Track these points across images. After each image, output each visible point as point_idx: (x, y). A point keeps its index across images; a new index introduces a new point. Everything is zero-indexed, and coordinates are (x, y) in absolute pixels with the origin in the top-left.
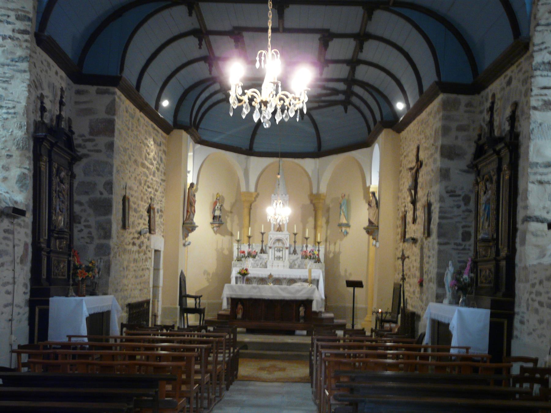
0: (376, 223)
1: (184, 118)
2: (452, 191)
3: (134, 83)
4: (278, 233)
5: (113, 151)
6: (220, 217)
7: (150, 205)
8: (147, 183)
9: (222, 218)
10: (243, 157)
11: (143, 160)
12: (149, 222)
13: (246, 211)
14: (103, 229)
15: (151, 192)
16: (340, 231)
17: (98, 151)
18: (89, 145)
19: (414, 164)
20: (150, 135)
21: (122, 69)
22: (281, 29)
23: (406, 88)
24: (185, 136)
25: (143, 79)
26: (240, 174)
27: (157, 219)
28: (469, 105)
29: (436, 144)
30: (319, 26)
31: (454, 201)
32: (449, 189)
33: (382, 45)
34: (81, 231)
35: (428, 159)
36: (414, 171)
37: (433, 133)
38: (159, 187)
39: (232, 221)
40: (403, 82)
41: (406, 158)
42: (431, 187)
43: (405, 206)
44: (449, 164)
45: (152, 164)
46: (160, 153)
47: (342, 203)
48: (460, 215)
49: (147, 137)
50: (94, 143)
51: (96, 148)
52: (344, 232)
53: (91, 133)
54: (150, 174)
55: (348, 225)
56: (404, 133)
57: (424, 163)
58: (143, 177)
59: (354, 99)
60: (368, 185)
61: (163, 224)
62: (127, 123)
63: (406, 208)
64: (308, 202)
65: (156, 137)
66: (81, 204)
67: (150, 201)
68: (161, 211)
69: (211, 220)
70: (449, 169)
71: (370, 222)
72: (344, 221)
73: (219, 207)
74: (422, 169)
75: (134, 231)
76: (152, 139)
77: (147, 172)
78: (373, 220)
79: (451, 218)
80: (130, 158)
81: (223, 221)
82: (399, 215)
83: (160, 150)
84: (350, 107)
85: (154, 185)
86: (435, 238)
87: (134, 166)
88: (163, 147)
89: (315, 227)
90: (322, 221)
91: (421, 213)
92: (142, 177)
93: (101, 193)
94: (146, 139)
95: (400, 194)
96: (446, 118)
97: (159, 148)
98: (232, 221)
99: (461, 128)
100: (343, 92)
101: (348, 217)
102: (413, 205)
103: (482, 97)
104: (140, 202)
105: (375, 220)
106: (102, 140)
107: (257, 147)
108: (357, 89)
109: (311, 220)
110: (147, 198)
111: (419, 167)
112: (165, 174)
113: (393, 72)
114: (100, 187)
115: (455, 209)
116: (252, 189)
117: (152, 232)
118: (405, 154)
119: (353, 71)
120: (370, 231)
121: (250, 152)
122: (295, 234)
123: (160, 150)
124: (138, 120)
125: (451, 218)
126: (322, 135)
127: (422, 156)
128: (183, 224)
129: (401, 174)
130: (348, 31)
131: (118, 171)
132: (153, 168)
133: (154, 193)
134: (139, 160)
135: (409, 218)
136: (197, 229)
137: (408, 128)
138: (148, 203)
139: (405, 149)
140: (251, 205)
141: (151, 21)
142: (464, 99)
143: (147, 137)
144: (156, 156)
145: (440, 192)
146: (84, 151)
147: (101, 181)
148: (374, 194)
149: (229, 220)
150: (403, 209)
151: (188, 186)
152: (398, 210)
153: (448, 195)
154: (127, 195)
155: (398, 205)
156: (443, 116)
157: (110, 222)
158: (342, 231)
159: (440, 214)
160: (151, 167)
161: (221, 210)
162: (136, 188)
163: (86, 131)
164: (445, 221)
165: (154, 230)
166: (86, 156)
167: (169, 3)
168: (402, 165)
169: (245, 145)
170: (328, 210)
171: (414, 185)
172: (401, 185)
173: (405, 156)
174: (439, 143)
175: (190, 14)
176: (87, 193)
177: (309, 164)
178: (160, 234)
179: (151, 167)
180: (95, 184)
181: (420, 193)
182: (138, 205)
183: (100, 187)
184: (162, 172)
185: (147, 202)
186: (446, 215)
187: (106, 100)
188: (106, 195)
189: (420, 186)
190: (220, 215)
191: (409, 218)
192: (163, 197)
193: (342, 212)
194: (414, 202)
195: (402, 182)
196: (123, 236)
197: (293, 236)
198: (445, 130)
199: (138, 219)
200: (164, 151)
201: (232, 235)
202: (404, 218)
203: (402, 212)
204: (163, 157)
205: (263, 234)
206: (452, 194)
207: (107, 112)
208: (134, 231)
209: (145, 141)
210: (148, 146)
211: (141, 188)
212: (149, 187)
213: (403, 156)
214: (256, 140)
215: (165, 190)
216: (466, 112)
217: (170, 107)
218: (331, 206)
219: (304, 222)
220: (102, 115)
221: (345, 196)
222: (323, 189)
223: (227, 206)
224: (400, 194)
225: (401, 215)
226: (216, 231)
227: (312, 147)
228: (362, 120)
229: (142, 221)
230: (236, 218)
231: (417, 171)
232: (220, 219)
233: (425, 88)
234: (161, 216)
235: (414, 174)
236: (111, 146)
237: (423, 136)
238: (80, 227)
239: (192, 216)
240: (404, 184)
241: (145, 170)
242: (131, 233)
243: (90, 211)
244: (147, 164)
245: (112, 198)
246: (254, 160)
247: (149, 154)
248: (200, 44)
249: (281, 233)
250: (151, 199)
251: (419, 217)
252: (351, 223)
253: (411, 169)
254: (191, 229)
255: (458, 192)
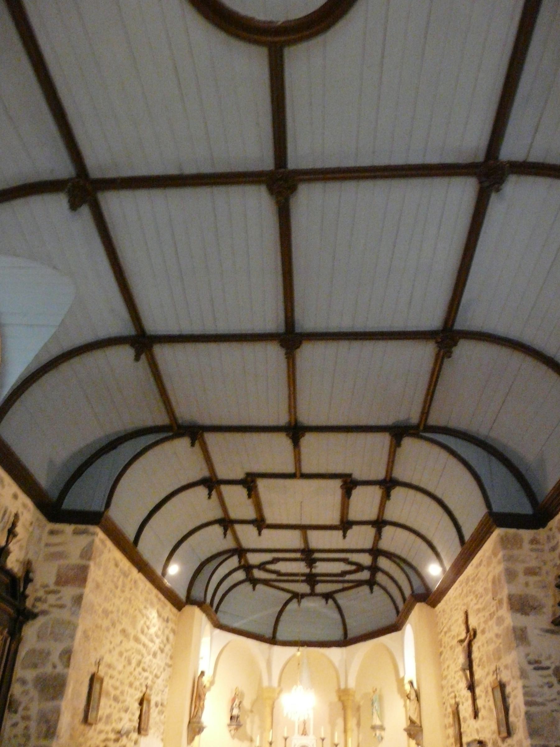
0: (418, 721)
1: (198, 593)
2: (536, 662)
3: (131, 537)
4: (303, 737)
5: (80, 607)
6: (238, 717)
7: (144, 695)
8: (142, 665)
9: (240, 719)
10: (265, 646)
11: (137, 632)
12: (140, 717)
13: (268, 710)
14: (47, 721)
15: (146, 678)
16: (374, 735)
17: (62, 607)
18: (52, 599)
19: (463, 635)
20: (152, 604)
21: (108, 505)
22: (298, 475)
23: (439, 549)
24: (197, 611)
25: (144, 531)
26: (263, 665)
27: (154, 714)
28: (534, 541)
29: (499, 597)
30: (340, 469)
31: (541, 676)
32: (532, 657)
33: (412, 492)
34: (15, 725)
35: (486, 622)
36: (466, 643)
37: (490, 585)
38: (161, 673)
39: (252, 722)
40: (435, 543)
41: (448, 635)
42: (499, 659)
43: (455, 697)
44: (523, 620)
45: (152, 641)
46: (167, 632)
47: (374, 699)
48: (555, 699)
49: (148, 606)
50: (58, 596)
51: (59, 602)
52: (378, 737)
53: (57, 583)
54: (149, 654)
55: (382, 728)
56: (440, 606)
57: (478, 632)
58: (134, 654)
59: (380, 577)
60: (401, 675)
61: (164, 723)
62: (115, 579)
63: (457, 700)
64: (335, 698)
65: (161, 610)
66: (24, 682)
67: (144, 689)
68: (162, 705)
69: (228, 720)
70: (526, 628)
71: (412, 722)
72: (377, 722)
73: (238, 704)
74: (476, 640)
75: (109, 728)
76: (156, 611)
77: (144, 651)
78: (415, 718)
79: (543, 704)
80: (113, 624)
81: (242, 722)
82: (446, 710)
83: (167, 627)
84: (376, 588)
85: (153, 668)
86: (523, 737)
87: (120, 638)
88: (171, 625)
89: (345, 731)
90: (352, 723)
91: (485, 702)
92: (133, 653)
93: (54, 667)
94: (145, 607)
95: (444, 682)
96: (509, 559)
97: (165, 624)
98: (252, 722)
99: (530, 572)
100: (369, 568)
101: (381, 717)
102: (471, 692)
103: (551, 529)
104: (126, 688)
105: (417, 718)
106: (68, 592)
107: (280, 636)
108: (383, 562)
109: (340, 722)
110: (141, 684)
111: (472, 637)
112: (171, 658)
113: (423, 531)
114: (55, 657)
115: (546, 689)
116: (275, 683)
117: (142, 732)
118: (445, 629)
119: (378, 535)
120: (412, 733)
121: (273, 640)
122: (323, 740)
123: (167, 627)
124: (135, 582)
125: (543, 704)
126: (347, 621)
127: (473, 623)
128: (189, 722)
129: (442, 656)
130: (373, 477)
131: (86, 636)
132: (154, 647)
133: (153, 679)
134: (131, 632)
135: (466, 710)
136: (205, 730)
137: (446, 598)
138: (141, 692)
139: (444, 625)
140: (273, 704)
141: (150, 454)
142: (526, 534)
143: (148, 606)
144: (160, 633)
145: (519, 663)
146: (44, 607)
147: (56, 649)
148: (411, 683)
149: (248, 721)
150: (453, 702)
151: (199, 673)
152: (444, 703)
153: (532, 667)
154: (99, 672)
155: (443, 697)
156: (504, 556)
157: (57, 712)
158: (375, 735)
159: (527, 698)
160: (151, 645)
161: (239, 708)
162: (120, 667)
163: (51, 580)
164: (533, 709)
165: (146, 730)
166: (44, 613)
167: (171, 434)
168: (443, 645)
169: (268, 633)
170: (358, 709)
171: (467, 663)
172: (444, 670)
173: (446, 633)
174: (504, 594)
175: (193, 445)
176: (35, 666)
177: (335, 653)
178: (158, 737)
179: (151, 645)
180: (48, 654)
181: (478, 673)
182: (122, 693)
183: (55, 657)
184: (167, 655)
185: (140, 690)
186: (534, 699)
187: (83, 541)
188: (60, 669)
189: (477, 664)
190: (239, 714)
191: (466, 710)
192: (166, 686)
193: (374, 709)
194: (471, 687)
195: (446, 666)
196: (84, 735)
197: (320, 741)
198: (511, 575)
199: (119, 711)
200: (174, 631)
201: (251, 740)
202: (456, 714)
203: (451, 706)
204: (171, 637)
205: (286, 739)
206: (536, 665)
207: (82, 556)
208: (109, 728)
209: (144, 611)
210: (148, 618)
211: (130, 669)
212: (144, 670)
213: (443, 633)
214: (280, 628)
215: (170, 677)
216: (532, 550)
217: (181, 574)
218: (362, 703)
219: (333, 724)
220: (74, 559)
221: (376, 689)
222: (352, 684)
223: (247, 704)
224: (444, 682)
225: (449, 710)
226: (234, 735)
227: (338, 635)
228: (389, 601)
229: (126, 717)
230: (257, 719)
231: (470, 645)
232: (238, 719)
233: (467, 537)
234: (161, 712)
235: (466, 647)
236: (78, 600)
237: (471, 596)
238: (16, 718)
239: (200, 713)
240: (448, 667)
241: (140, 647)
242: (101, 732)
243: (34, 693)
244: (143, 638)
245: (67, 673)
246: (277, 649)
247: (148, 628)
248: (210, 495)
249: (306, 737)
250: (147, 687)
251: (482, 708)
252: (386, 725)
253: (461, 641)
254: (197, 730)
255: (546, 663)
